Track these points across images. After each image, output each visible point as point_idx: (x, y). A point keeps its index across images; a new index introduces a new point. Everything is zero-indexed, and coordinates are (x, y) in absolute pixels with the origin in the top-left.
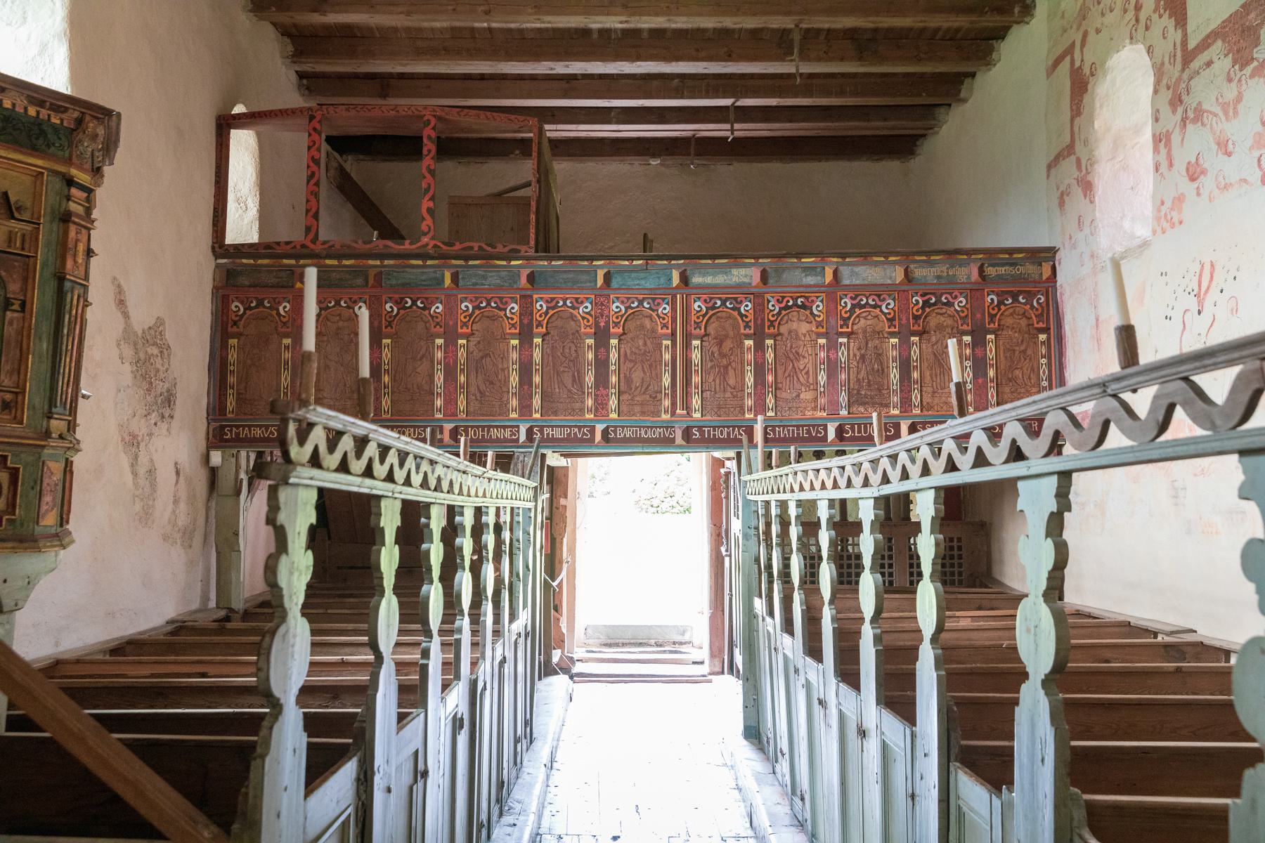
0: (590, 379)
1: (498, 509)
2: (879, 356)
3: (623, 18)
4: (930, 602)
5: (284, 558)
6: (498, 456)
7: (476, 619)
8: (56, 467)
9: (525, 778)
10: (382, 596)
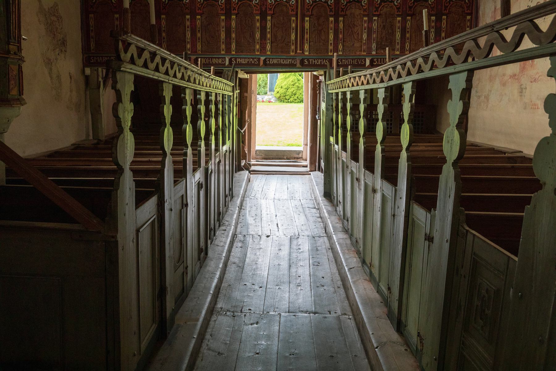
0: (258, 35)
1: (216, 94)
2: (392, 26)
4: (407, 132)
5: (120, 104)
7: (208, 145)
8: (15, 68)
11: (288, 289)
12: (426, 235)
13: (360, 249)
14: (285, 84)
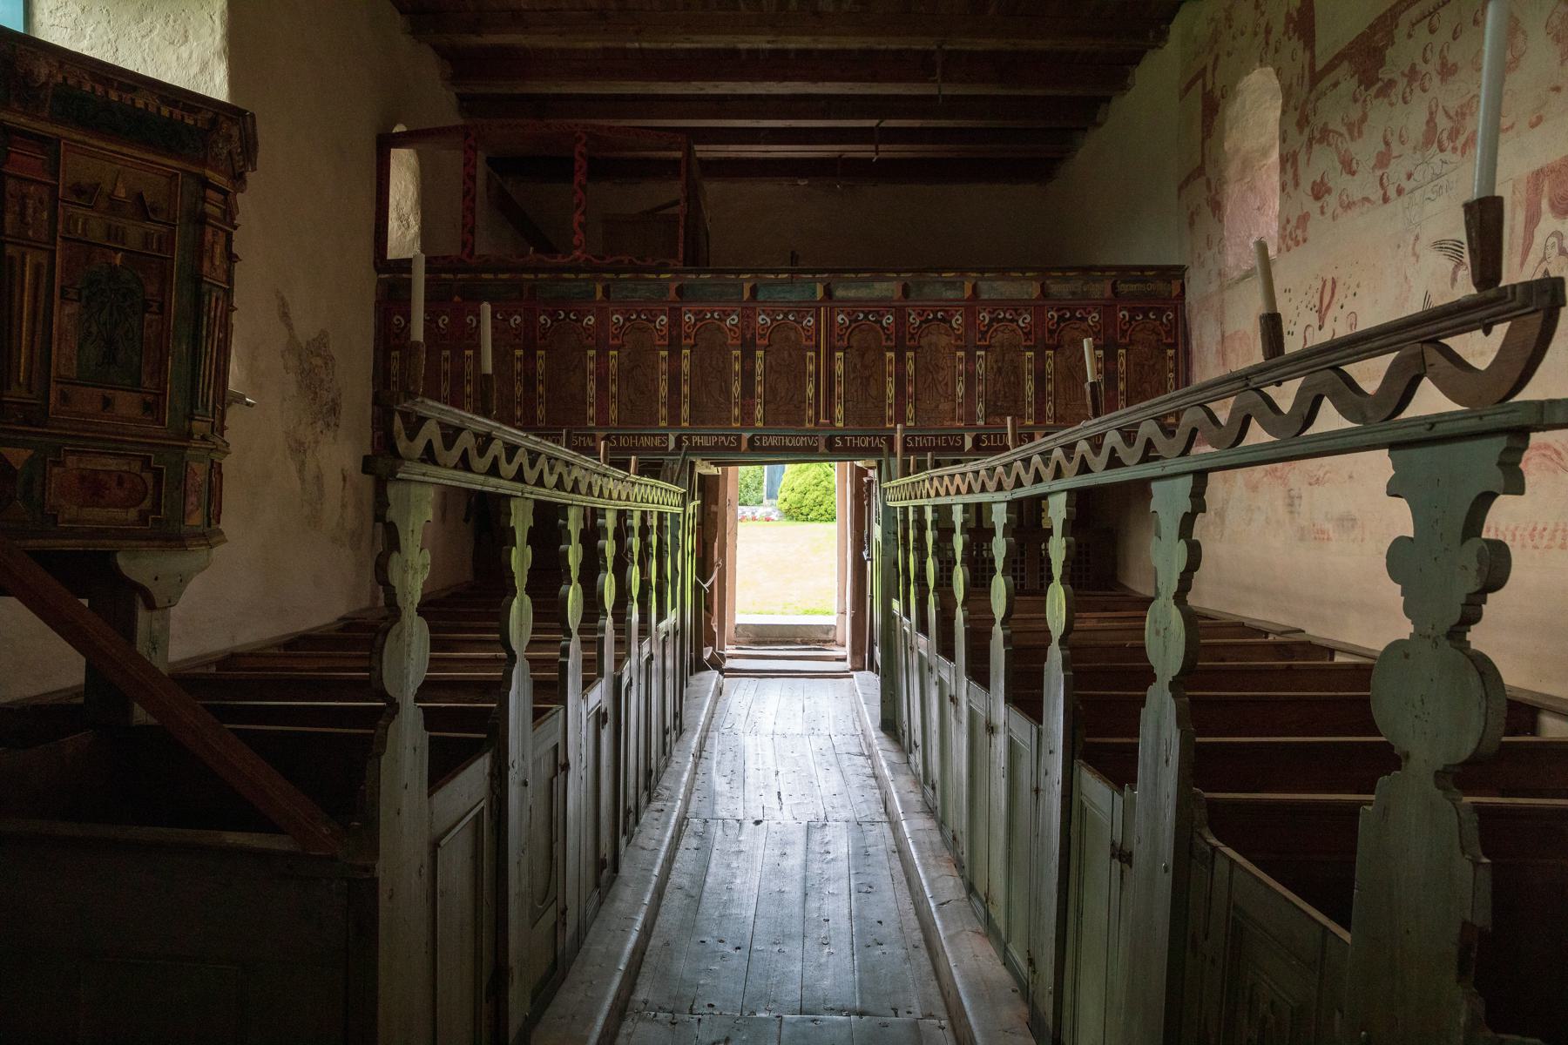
0: (736, 389)
2: (1017, 370)
3: (770, 38)
4: (1513, 211)
5: (395, 555)
6: (640, 463)
9: (674, 766)
10: (514, 595)
11: (799, 952)
12: (1113, 845)
13: (962, 858)
14: (799, 483)
